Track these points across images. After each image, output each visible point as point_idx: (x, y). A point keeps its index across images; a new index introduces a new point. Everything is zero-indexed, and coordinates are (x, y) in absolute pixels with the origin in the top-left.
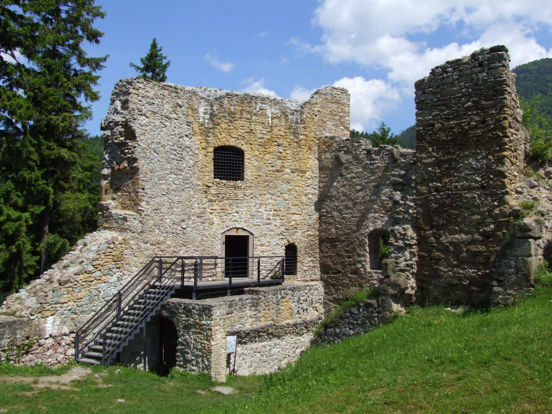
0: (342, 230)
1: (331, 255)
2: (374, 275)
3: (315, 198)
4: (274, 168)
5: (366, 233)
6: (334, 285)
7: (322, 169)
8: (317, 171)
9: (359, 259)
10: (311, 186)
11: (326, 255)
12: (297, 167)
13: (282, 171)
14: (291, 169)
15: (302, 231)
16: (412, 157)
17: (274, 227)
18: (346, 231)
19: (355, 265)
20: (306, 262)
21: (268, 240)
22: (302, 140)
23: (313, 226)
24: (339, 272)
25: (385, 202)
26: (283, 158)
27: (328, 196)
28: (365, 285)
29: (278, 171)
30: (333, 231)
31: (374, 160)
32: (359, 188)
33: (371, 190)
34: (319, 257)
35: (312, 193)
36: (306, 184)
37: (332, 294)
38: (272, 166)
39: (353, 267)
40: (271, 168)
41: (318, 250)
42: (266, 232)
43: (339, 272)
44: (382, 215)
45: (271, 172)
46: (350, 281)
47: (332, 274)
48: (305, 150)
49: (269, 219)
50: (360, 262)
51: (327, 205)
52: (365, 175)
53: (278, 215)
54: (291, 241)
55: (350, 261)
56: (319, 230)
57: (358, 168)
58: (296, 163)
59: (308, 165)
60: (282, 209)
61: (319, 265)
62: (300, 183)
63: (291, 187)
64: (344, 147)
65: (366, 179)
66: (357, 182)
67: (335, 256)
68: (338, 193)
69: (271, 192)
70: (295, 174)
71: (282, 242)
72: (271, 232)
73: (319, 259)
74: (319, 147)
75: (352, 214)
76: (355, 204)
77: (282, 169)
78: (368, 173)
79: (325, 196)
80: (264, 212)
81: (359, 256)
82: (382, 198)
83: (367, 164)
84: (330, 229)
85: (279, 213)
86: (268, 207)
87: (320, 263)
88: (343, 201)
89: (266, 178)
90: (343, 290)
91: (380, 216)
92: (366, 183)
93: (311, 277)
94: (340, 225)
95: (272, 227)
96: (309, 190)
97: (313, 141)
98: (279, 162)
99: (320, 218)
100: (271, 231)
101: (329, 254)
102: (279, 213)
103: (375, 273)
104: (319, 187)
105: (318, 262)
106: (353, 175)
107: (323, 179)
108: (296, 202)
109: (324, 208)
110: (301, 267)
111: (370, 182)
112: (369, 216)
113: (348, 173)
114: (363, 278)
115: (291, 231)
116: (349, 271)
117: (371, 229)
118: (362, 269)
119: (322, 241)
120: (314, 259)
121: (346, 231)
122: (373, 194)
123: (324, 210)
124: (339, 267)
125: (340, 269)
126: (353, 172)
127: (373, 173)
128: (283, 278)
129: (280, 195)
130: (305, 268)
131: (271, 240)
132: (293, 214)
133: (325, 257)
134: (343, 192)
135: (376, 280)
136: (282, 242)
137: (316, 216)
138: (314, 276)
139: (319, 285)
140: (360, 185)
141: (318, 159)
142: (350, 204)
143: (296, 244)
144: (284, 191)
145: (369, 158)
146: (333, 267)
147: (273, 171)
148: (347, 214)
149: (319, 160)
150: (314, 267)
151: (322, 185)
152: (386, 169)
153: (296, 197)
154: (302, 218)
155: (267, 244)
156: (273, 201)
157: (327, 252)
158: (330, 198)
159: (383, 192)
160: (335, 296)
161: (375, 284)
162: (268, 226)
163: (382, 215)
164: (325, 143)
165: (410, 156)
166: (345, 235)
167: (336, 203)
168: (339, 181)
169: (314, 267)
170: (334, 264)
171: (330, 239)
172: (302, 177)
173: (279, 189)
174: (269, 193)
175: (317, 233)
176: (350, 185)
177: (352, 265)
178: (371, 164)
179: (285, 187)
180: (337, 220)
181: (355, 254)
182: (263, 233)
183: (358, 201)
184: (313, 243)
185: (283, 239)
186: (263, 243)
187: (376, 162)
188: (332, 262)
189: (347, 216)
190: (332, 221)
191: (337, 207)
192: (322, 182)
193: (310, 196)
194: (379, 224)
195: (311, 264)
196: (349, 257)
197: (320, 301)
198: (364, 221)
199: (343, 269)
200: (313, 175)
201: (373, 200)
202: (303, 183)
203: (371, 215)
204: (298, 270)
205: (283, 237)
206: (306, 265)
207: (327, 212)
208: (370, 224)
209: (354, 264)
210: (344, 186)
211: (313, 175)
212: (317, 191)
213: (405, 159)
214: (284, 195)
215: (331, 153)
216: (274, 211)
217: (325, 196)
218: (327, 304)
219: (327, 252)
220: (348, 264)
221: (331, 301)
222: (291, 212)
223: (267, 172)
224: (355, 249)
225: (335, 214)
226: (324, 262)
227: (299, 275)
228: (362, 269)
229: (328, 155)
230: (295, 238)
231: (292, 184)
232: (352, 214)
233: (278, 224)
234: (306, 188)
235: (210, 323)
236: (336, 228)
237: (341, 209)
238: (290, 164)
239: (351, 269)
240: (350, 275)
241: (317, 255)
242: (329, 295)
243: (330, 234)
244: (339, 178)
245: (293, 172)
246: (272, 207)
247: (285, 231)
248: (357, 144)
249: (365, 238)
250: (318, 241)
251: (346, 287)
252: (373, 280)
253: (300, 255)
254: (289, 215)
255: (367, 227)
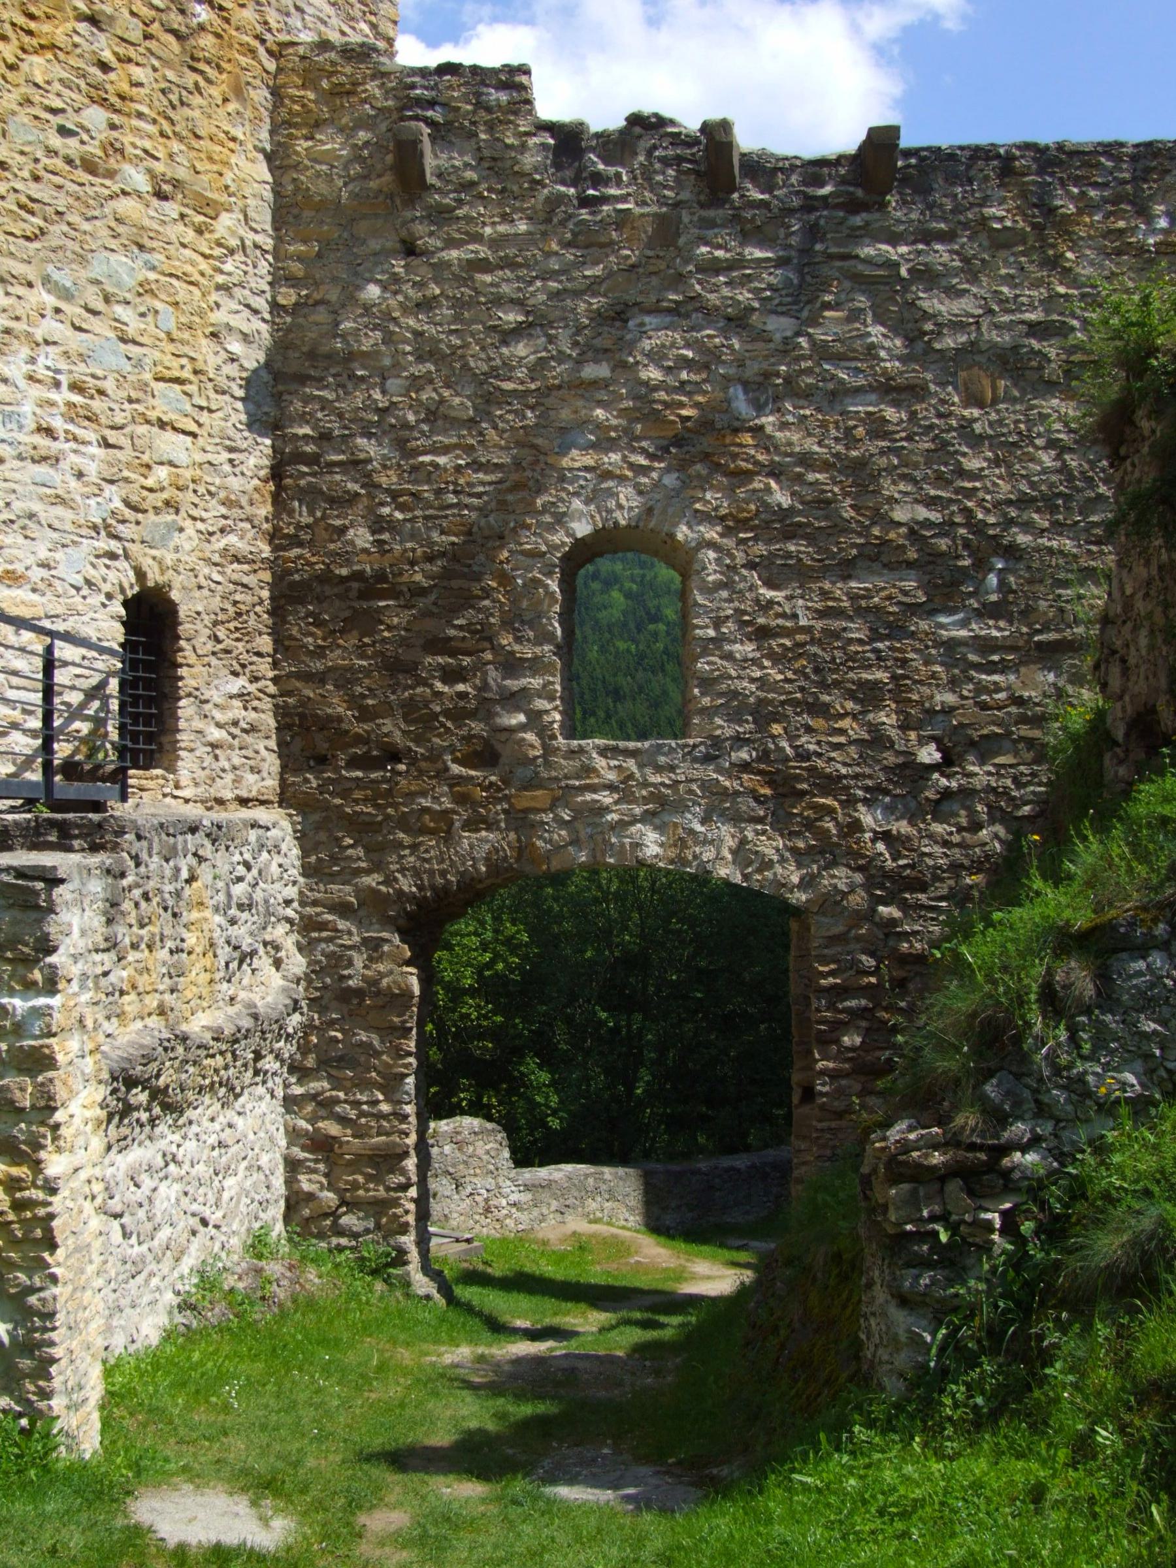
0: (413, 536)
1: (350, 668)
2: (600, 763)
3: (253, 358)
4: (73, 142)
5: (553, 547)
6: (361, 827)
7: (288, 211)
8: (264, 218)
9: (513, 684)
10: (237, 292)
11: (318, 665)
12: (182, 173)
13: (111, 174)
14: (149, 171)
15: (200, 526)
16: (804, 183)
17: (73, 483)
18: (435, 536)
19: (489, 716)
20: (217, 699)
21: (43, 554)
22: (202, 27)
23: (249, 510)
24: (394, 756)
25: (662, 395)
26: (114, 99)
27: (330, 357)
28: (548, 817)
29: (90, 167)
30: (362, 537)
31: (598, 180)
32: (512, 317)
33: (579, 330)
34: (275, 680)
35: (243, 336)
36: (220, 279)
37: (350, 874)
38: (63, 131)
39: (477, 727)
40: (56, 141)
41: (265, 643)
42: (37, 507)
43: (394, 756)
44: (642, 461)
45: (58, 163)
46: (462, 799)
47: (353, 763)
48: (215, 92)
49: (49, 432)
50: (515, 700)
51: (324, 404)
52: (548, 254)
53: (92, 418)
54: (154, 577)
55: (463, 696)
56: (273, 537)
57: (506, 218)
58: (176, 146)
59: (228, 178)
60: (109, 385)
61: (273, 723)
62: (193, 263)
63: (152, 276)
64: (432, 104)
65: (546, 275)
66: (505, 289)
67: (367, 672)
68: (389, 338)
69: (56, 276)
70: (172, 209)
71: (112, 576)
72: (60, 511)
73: (272, 689)
74: (276, 92)
75: (469, 449)
76: (489, 399)
77: (112, 163)
78: (568, 245)
79: (312, 355)
80: (22, 383)
81: (512, 665)
82: (644, 375)
83: (556, 201)
84: (343, 530)
85: (97, 405)
86: (41, 361)
87: (281, 712)
88: (417, 384)
89: (35, 190)
90: (414, 847)
91: (632, 466)
92: (556, 295)
93: (237, 781)
94: (402, 508)
95: (61, 479)
96: (227, 314)
97: (252, 52)
98: (96, 117)
99: (277, 473)
100: (60, 501)
101: (335, 658)
102: (97, 405)
103: (603, 752)
104: (274, 306)
105: (267, 704)
106: (484, 252)
107: (296, 268)
108: (175, 363)
109: (304, 419)
110: (198, 724)
111: (577, 294)
112: (565, 462)
113: (451, 243)
114: (533, 783)
115: (151, 515)
116: (452, 749)
117: (582, 529)
118: (530, 737)
119: (288, 595)
120: (252, 688)
121: (435, 536)
122: (590, 352)
123: (306, 430)
124: (392, 729)
125: (398, 737)
126: (477, 238)
127: (589, 242)
128: (119, 777)
129: (100, 305)
130: (216, 734)
131: (59, 555)
132: (162, 424)
133: (307, 677)
134: (418, 334)
135: (611, 787)
136: (112, 576)
137: (258, 455)
138: (251, 778)
139: (281, 825)
140: (518, 303)
141: (269, 158)
142: (460, 402)
143: (175, 595)
144: (118, 285)
145: (569, 173)
146: (360, 729)
147: (69, 161)
148: (445, 450)
149: (277, 159)
150: (252, 729)
151: (288, 296)
152: (666, 231)
153: (176, 334)
154: (199, 457)
155: (37, 574)
156: (70, 333)
157: (319, 653)
158: (344, 366)
159: (647, 344)
160: (371, 880)
161: (607, 809)
162: (42, 470)
163: (642, 461)
164: (310, 76)
165: (794, 179)
166: (430, 559)
167: (377, 395)
168: (396, 279)
169: (252, 729)
170: (365, 715)
171: (343, 580)
172: (199, 231)
173: (97, 269)
174: (46, 280)
175: (266, 551)
176: (459, 304)
177: (473, 715)
178: (585, 202)
179: (124, 269)
180: (383, 481)
181: (488, 656)
182: (17, 506)
183: (508, 386)
184: (249, 599)
185: (113, 556)
186: (19, 568)
187: (613, 191)
188: (354, 701)
189: (442, 460)
190: (353, 487)
191: (383, 412)
192: (292, 281)
193: (236, 347)
194: (626, 503)
195: (236, 710)
196: (451, 675)
197: (290, 912)
198: (540, 490)
199: (418, 740)
200: (250, 237)
201: (594, 384)
202: (204, 265)
203: (577, 459)
204: (184, 738)
205: (114, 546)
206: (219, 716)
207: (325, 437)
208: (577, 504)
209: (484, 708)
210: (426, 305)
211: (250, 237)
212: (264, 327)
213: (769, 189)
214: (119, 310)
215: (347, 132)
216: (75, 387)
217: (312, 355)
218: (323, 926)
219: (319, 653)
220: (447, 713)
221: (343, 909)
222: (152, 415)
223: (39, 154)
224: (484, 635)
225: (368, 447)
226: (305, 702)
227: (187, 766)
228: (530, 737)
229: (331, 143)
230: (169, 558)
231: (157, 258)
232: (469, 449)
233: (92, 470)
234: (214, 297)
235: (37, 1012)
236: (378, 525)
237: (405, 425)
238: (148, 144)
239: (468, 739)
240: (456, 769)
241: (264, 667)
242: (332, 878)
243: (345, 557)
244: (398, 266)
245: (161, 195)
246: (63, 366)
247: (128, 513)
248: (503, 97)
249: (549, 574)
250: (265, 594)
251: (432, 832)
252: (593, 789)
253: (192, 659)
254: (142, 429)
255: (560, 519)
